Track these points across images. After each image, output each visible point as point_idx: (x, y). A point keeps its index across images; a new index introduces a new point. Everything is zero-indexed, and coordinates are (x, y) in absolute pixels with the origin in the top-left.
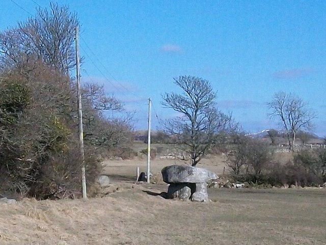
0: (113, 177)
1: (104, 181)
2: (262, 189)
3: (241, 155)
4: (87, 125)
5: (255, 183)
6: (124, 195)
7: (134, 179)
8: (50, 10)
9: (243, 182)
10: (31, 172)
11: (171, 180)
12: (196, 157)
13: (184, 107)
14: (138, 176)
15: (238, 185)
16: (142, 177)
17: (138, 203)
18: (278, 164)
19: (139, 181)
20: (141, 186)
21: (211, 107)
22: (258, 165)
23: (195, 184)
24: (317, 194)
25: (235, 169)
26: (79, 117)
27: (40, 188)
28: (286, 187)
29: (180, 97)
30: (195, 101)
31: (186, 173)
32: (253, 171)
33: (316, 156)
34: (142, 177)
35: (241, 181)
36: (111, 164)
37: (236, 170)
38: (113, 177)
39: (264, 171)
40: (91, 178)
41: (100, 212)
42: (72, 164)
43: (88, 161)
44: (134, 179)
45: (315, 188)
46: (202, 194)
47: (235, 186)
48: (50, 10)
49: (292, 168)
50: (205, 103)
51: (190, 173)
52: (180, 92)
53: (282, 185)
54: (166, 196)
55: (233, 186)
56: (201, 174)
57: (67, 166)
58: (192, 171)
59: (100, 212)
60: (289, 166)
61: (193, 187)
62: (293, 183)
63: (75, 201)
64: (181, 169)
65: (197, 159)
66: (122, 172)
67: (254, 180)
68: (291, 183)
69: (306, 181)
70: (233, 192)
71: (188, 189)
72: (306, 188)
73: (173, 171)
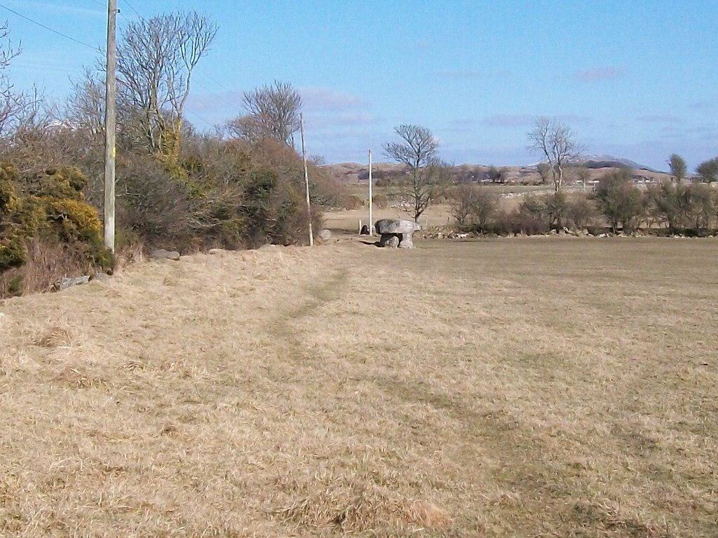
0: (334, 231)
1: (326, 234)
2: (487, 238)
3: (466, 205)
4: (312, 188)
5: (479, 232)
6: (343, 244)
7: (356, 232)
8: (275, 88)
9: (467, 232)
10: (275, 228)
11: (383, 232)
12: (419, 208)
13: (406, 157)
14: (361, 229)
15: (462, 235)
16: (365, 230)
17: (353, 249)
18: (503, 213)
19: (361, 234)
20: (364, 238)
21: (432, 157)
22: (482, 215)
23: (401, 234)
24: (540, 241)
25: (459, 219)
26: (306, 184)
27: (279, 238)
28: (511, 236)
29: (401, 147)
30: (416, 150)
31: (394, 225)
32: (478, 221)
33: (541, 203)
34: (365, 230)
35: (465, 231)
36: (332, 217)
37: (460, 220)
38: (334, 231)
39: (490, 221)
40: (316, 233)
41: (325, 252)
42: (301, 222)
43: (313, 218)
44: (356, 232)
45: (540, 236)
46: (408, 242)
47: (459, 236)
48: (275, 88)
49: (519, 216)
50: (426, 152)
51: (398, 225)
52: (403, 142)
53: (508, 233)
54: (378, 244)
55: (457, 236)
56: (406, 226)
57: (298, 222)
58: (399, 224)
59: (325, 252)
60: (515, 215)
61: (400, 236)
62: (519, 232)
63: (304, 248)
64: (390, 222)
65: (420, 210)
66: (344, 226)
67: (480, 230)
68: (516, 232)
69: (531, 230)
70: (457, 241)
71: (396, 238)
72: (533, 236)
73: (383, 224)
